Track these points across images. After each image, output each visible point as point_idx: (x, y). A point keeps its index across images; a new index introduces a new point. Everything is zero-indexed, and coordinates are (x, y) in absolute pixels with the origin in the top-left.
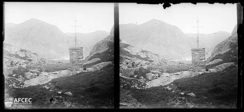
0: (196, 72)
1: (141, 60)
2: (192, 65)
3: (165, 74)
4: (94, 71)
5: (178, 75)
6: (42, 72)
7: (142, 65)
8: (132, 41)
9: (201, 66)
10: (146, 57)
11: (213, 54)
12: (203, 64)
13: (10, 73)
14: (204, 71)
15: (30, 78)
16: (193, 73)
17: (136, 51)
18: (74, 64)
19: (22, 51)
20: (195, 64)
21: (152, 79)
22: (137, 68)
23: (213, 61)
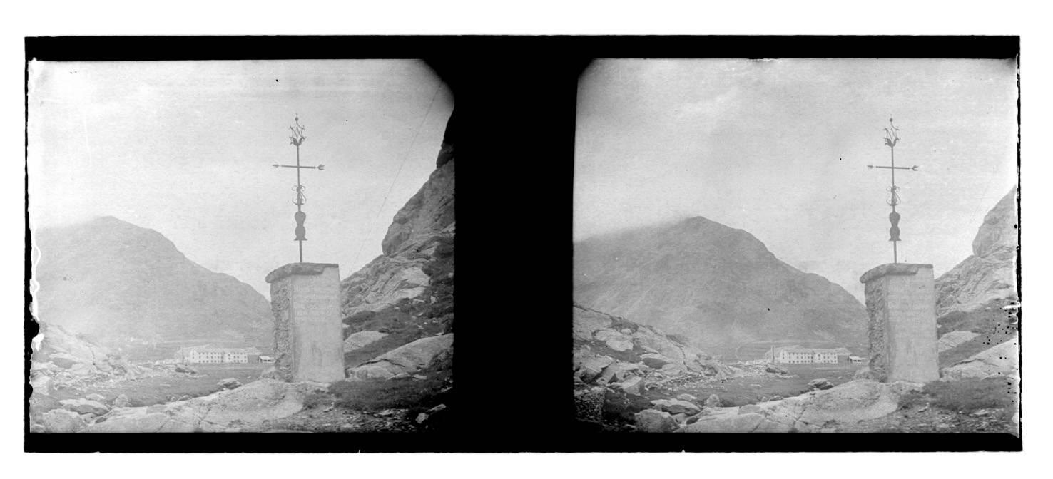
3: (715, 412)
7: (614, 379)
10: (630, 347)
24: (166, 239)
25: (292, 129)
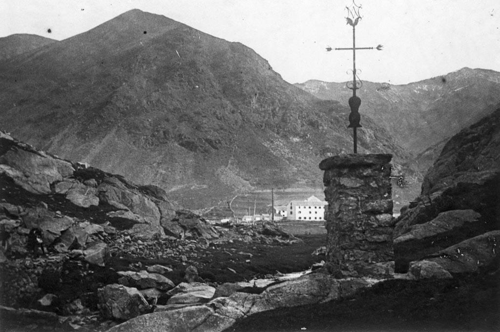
0: (349, 279)
1: (71, 219)
2: (324, 240)
4: (451, 276)
5: (259, 293)
6: (182, 284)
7: (76, 245)
8: (29, 121)
9: (373, 246)
10: (96, 202)
11: (428, 186)
12: (382, 238)
13: (23, 289)
14: (387, 271)
15: (127, 311)
16: (332, 282)
17: (47, 172)
18: (346, 243)
19: (82, 175)
20: (344, 235)
21: (127, 311)
22: (54, 258)
23: (434, 223)
24: (47, 38)
25: (348, 8)
